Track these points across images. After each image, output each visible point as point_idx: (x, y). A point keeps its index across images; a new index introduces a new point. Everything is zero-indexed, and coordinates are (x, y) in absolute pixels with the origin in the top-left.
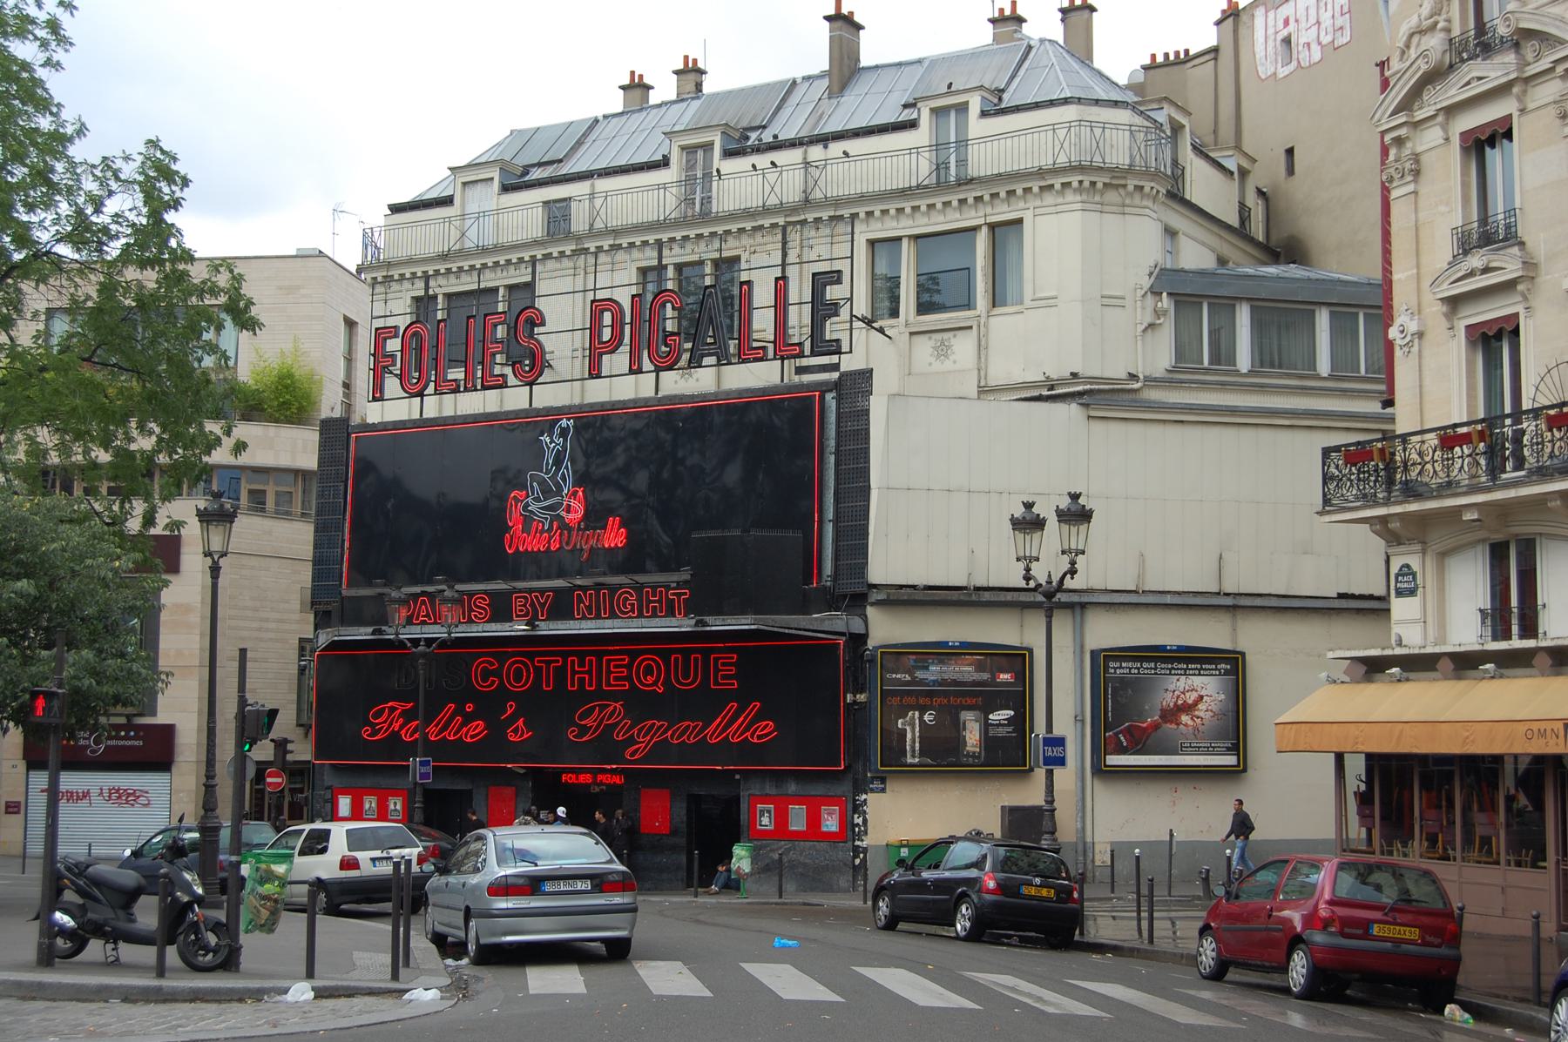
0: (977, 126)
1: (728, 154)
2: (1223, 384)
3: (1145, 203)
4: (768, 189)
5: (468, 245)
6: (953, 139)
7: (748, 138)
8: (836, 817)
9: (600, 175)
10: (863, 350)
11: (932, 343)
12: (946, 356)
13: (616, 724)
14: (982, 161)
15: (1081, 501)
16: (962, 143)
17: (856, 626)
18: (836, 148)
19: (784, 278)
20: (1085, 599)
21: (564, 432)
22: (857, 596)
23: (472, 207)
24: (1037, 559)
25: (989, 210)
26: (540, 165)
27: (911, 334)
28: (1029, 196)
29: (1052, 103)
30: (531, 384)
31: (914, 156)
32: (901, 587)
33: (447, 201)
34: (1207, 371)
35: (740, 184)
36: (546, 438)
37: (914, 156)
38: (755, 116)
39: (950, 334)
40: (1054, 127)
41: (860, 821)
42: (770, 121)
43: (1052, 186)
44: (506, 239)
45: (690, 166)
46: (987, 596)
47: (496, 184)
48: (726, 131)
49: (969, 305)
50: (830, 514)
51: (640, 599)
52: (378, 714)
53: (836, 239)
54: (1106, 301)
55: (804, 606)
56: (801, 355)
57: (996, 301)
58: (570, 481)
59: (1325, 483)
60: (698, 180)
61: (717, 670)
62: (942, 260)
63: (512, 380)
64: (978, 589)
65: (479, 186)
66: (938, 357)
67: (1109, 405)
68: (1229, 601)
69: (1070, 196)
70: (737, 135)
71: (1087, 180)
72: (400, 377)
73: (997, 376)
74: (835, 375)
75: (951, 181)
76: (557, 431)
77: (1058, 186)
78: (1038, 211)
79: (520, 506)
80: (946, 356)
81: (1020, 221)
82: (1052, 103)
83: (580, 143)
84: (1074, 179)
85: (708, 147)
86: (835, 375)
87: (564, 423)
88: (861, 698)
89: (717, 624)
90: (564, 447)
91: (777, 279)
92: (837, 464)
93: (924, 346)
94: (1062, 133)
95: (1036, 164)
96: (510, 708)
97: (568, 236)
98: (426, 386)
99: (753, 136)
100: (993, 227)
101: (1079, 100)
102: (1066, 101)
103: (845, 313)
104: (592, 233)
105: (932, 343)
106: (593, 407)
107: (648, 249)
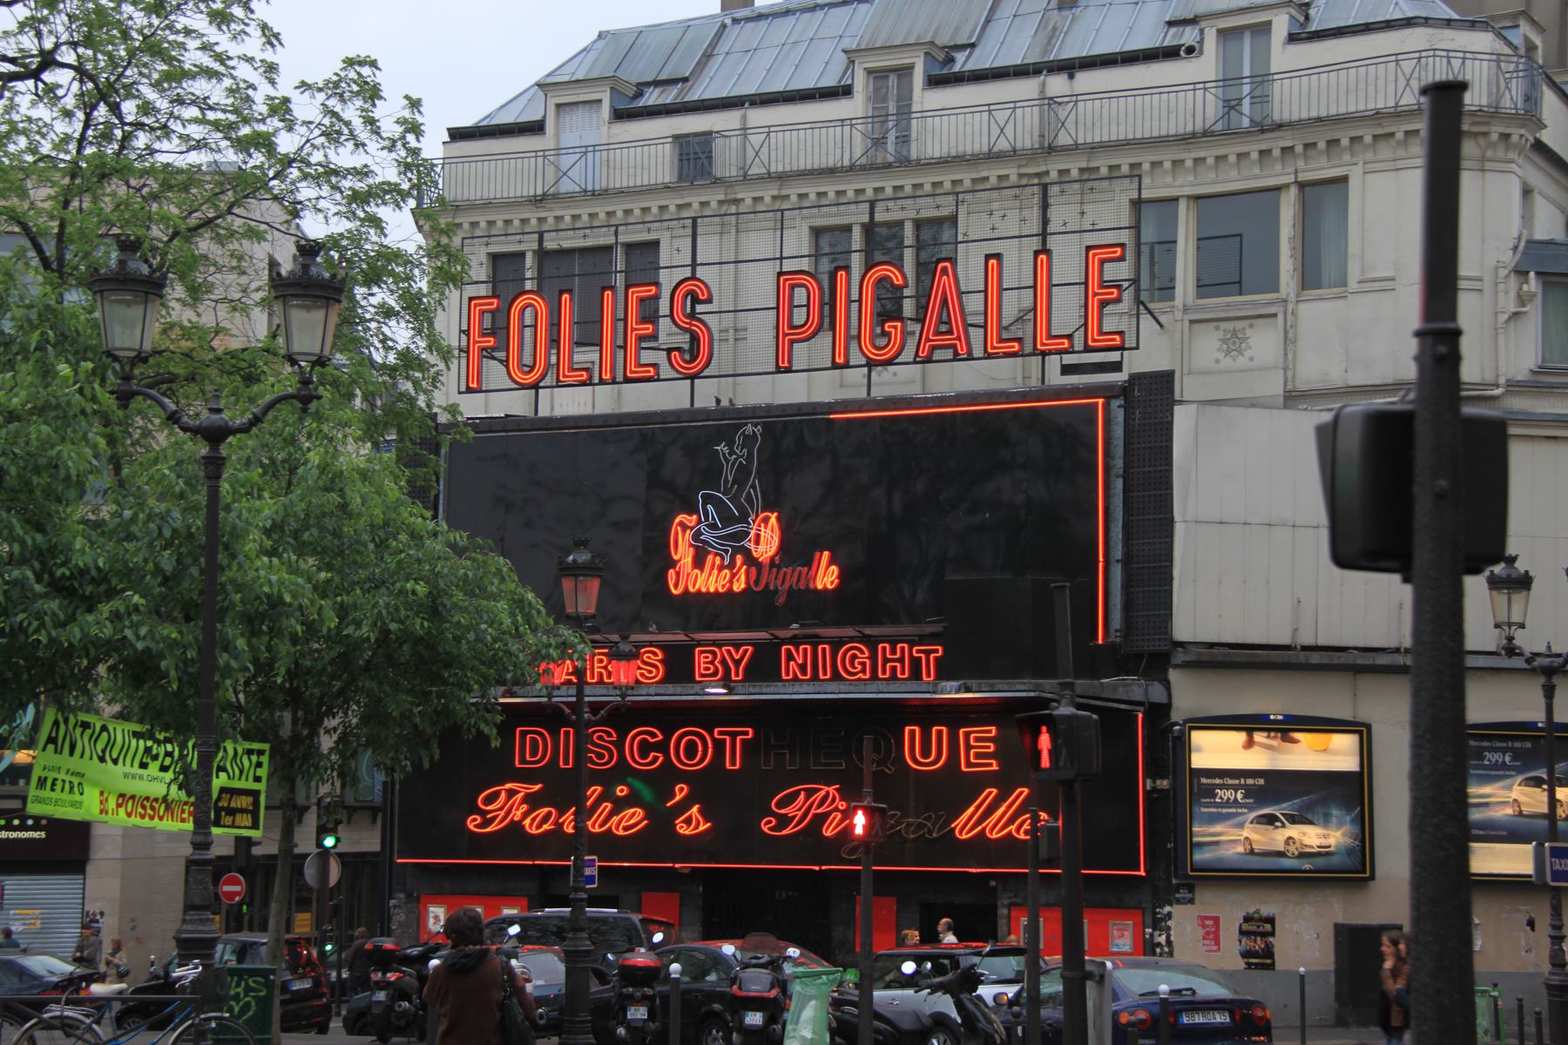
0: (1283, 56)
1: (934, 82)
3: (1512, 155)
4: (995, 131)
5: (566, 186)
6: (1247, 73)
7: (952, 60)
8: (1128, 934)
11: (1220, 334)
12: (1240, 352)
13: (826, 815)
14: (1289, 101)
16: (1262, 78)
17: (1156, 693)
18: (1088, 81)
19: (1045, 250)
21: (749, 440)
22: (1155, 653)
23: (570, 139)
24: (1522, 626)
26: (656, 83)
28: (1357, 147)
29: (1389, 25)
31: (1200, 93)
32: (1212, 645)
33: (536, 128)
35: (949, 121)
36: (722, 448)
37: (1200, 93)
38: (957, 30)
39: (1245, 323)
40: (1397, 57)
41: (1162, 939)
43: (1392, 135)
45: (878, 97)
46: (1315, 658)
51: (873, 658)
52: (491, 799)
56: (1069, 351)
57: (1310, 278)
60: (893, 116)
61: (968, 747)
63: (666, 371)
64: (1305, 648)
65: (581, 108)
66: (1228, 353)
70: (941, 56)
75: (1245, 122)
76: (738, 440)
77: (1400, 136)
78: (1370, 167)
80: (1240, 352)
81: (1344, 180)
82: (1389, 25)
83: (708, 56)
85: (905, 72)
87: (749, 429)
88: (1164, 784)
90: (750, 454)
95: (1371, 106)
96: (681, 792)
98: (543, 376)
99: (960, 57)
100: (1302, 186)
101: (1427, 22)
102: (1408, 23)
105: (1220, 334)
106: (785, 410)
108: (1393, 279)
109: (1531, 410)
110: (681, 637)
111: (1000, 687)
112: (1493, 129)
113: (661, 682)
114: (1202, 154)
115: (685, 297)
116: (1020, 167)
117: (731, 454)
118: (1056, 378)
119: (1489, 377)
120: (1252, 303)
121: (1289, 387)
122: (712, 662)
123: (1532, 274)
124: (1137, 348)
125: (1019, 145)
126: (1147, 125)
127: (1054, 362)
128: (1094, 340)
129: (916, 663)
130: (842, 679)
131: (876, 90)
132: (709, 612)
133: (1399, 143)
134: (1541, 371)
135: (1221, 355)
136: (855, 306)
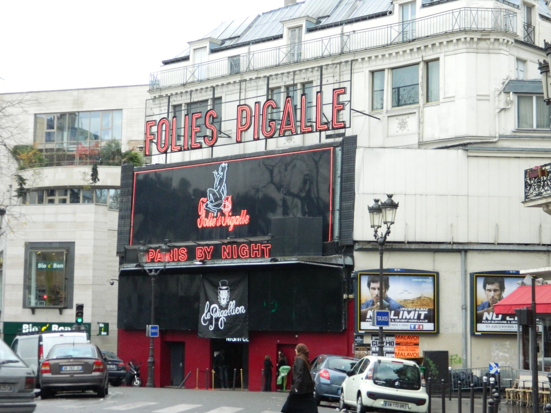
1: (310, 30)
2: (543, 137)
3: (501, 47)
4: (324, 47)
9: (253, 43)
10: (358, 127)
11: (398, 121)
12: (405, 128)
14: (422, 29)
15: (393, 198)
17: (348, 261)
20: (466, 247)
22: (349, 247)
23: (197, 61)
25: (424, 54)
27: (389, 117)
30: (212, 146)
31: (389, 29)
33: (186, 58)
34: (535, 131)
35: (314, 45)
38: (326, 11)
39: (406, 116)
40: (453, 11)
42: (332, 13)
43: (452, 41)
44: (211, 76)
45: (292, 37)
46: (413, 246)
47: (208, 50)
48: (308, 19)
49: (415, 102)
50: (337, 207)
51: (250, 250)
53: (162, 105)
54: (479, 98)
55: (325, 251)
56: (328, 129)
58: (225, 192)
59: (526, 187)
62: (405, 78)
63: (204, 145)
66: (401, 128)
67: (478, 150)
68: (545, 248)
69: (461, 46)
70: (315, 21)
71: (468, 37)
72: (157, 144)
73: (428, 136)
74: (340, 139)
76: (220, 169)
77: (455, 41)
78: (447, 54)
79: (205, 205)
81: (437, 59)
84: (462, 36)
86: (340, 139)
88: (351, 296)
89: (282, 261)
90: (223, 176)
91: (317, 93)
92: (341, 182)
93: (394, 123)
94: (456, 14)
95: (444, 30)
97: (238, 73)
100: (427, 63)
103: (347, 107)
104: (249, 71)
107: (236, 84)
108: (454, 97)
109: (511, 147)
110: (193, 244)
111: (287, 259)
112: (491, 37)
113: (186, 261)
114: (391, 52)
115: (210, 116)
116: (332, 60)
117: (218, 174)
118: (324, 141)
119: (493, 134)
120: (409, 108)
121: (421, 140)
122: (201, 253)
123: (511, 93)
124: (350, 127)
125: (331, 53)
126: (364, 44)
127: (323, 134)
128: (335, 125)
129: (263, 251)
130: (240, 258)
131: (292, 35)
132: (208, 233)
133: (455, 44)
134: (518, 131)
135: (398, 129)
136: (253, 118)
